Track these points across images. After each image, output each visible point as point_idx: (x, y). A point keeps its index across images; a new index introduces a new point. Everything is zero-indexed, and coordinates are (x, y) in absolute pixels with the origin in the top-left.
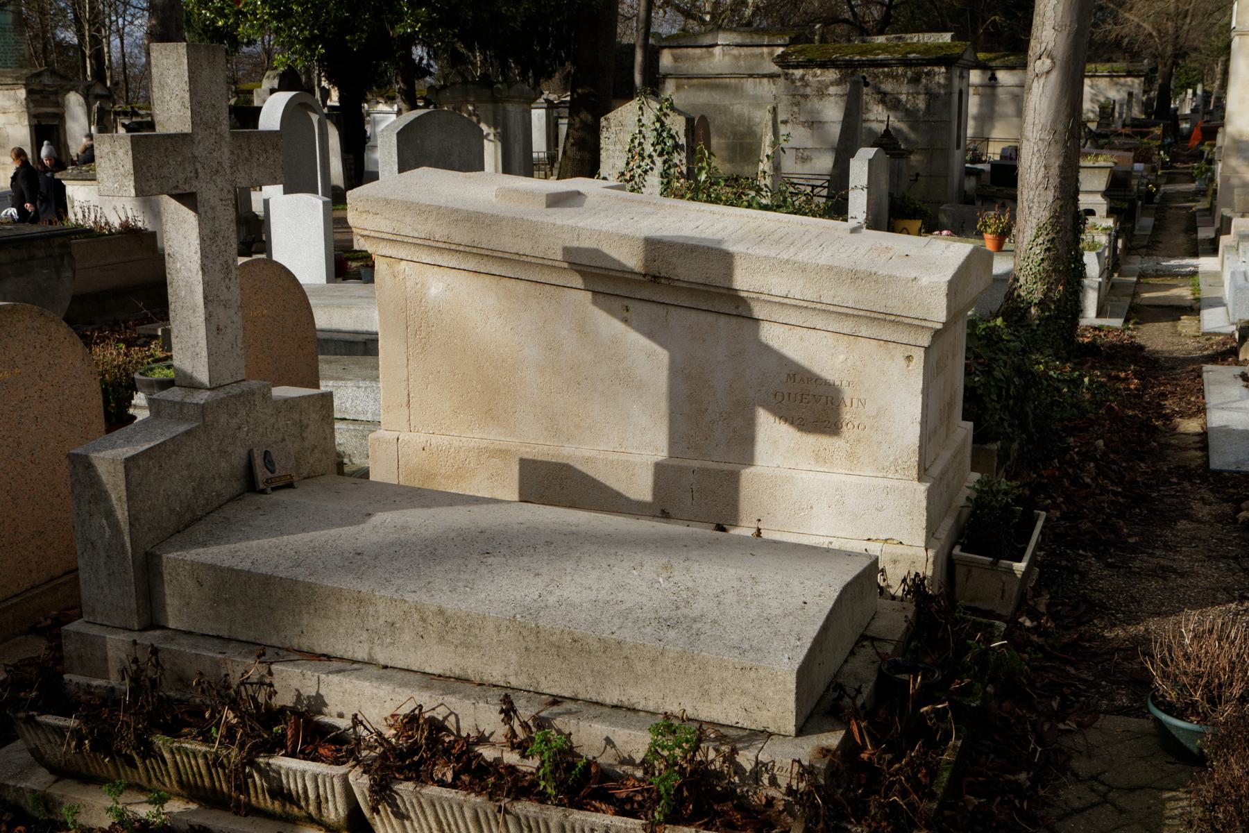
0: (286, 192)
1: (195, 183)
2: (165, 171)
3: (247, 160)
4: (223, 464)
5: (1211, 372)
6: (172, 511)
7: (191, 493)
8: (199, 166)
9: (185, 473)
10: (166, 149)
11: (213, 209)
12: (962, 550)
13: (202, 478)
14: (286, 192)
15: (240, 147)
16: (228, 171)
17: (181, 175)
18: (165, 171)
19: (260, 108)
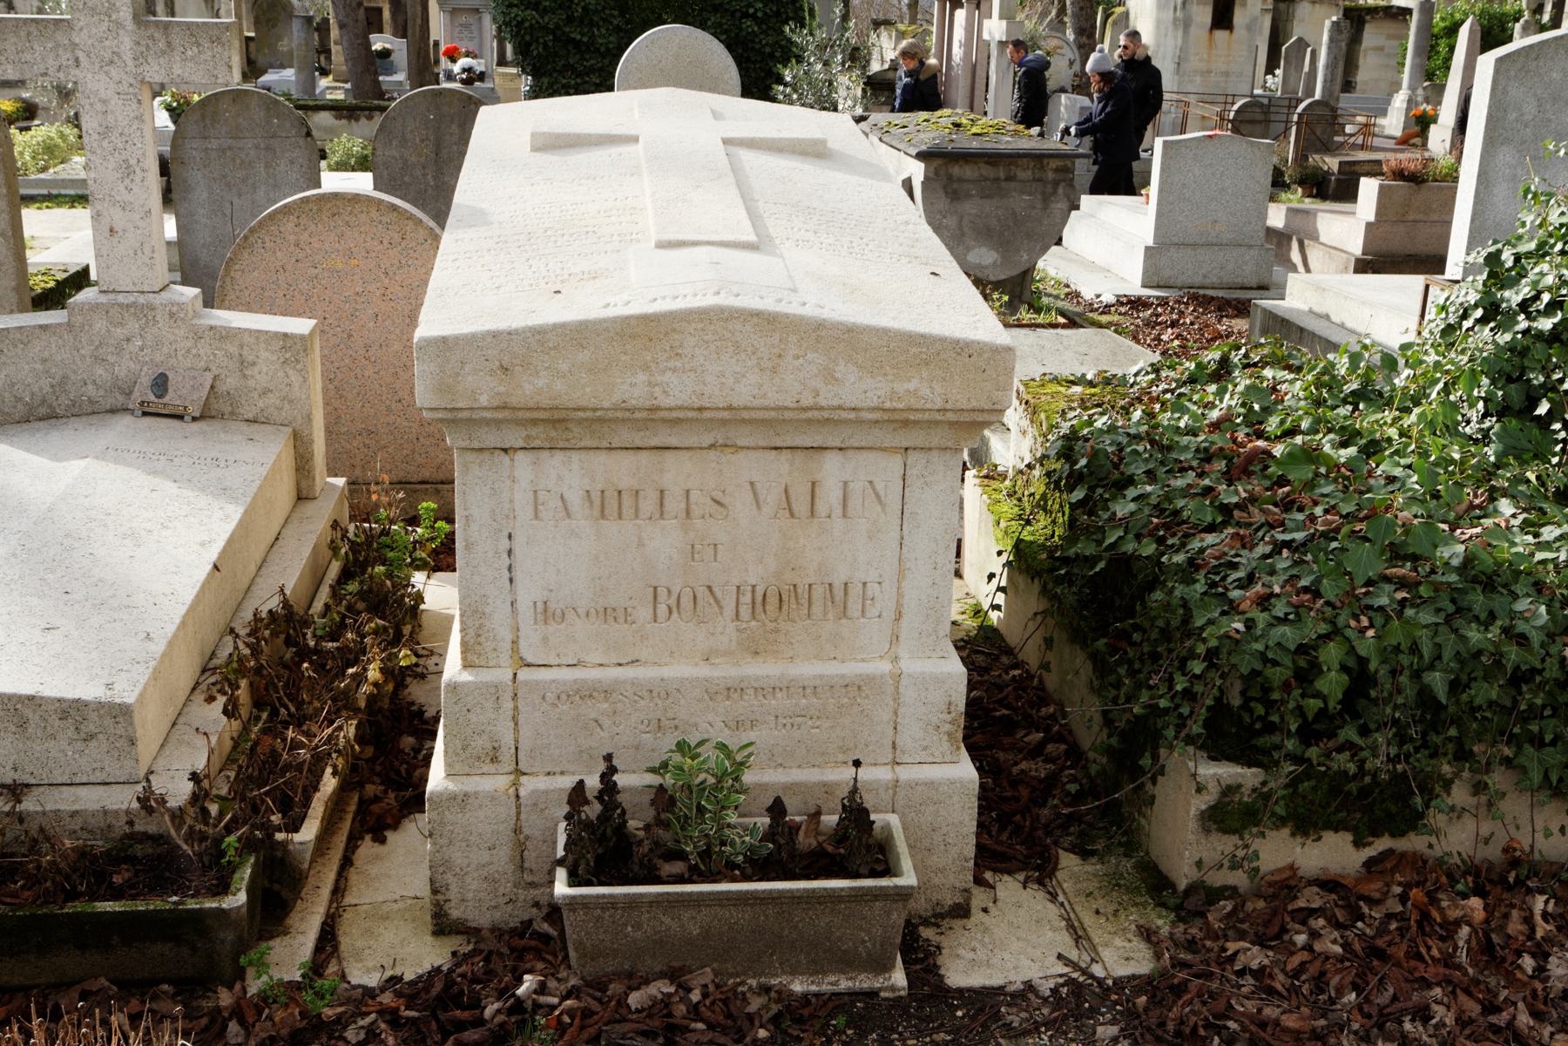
0: (1147, 248)
1: (74, 71)
2: (28, 56)
3: (164, 53)
4: (101, 372)
5: (197, 414)
6: (19, 399)
7: (47, 389)
8: (81, 55)
9: (39, 366)
10: (29, 34)
11: (104, 102)
12: (574, 880)
13: (65, 378)
14: (1147, 248)
15: (152, 37)
16: (130, 63)
17: (51, 62)
18: (28, 56)
19: (773, 100)
